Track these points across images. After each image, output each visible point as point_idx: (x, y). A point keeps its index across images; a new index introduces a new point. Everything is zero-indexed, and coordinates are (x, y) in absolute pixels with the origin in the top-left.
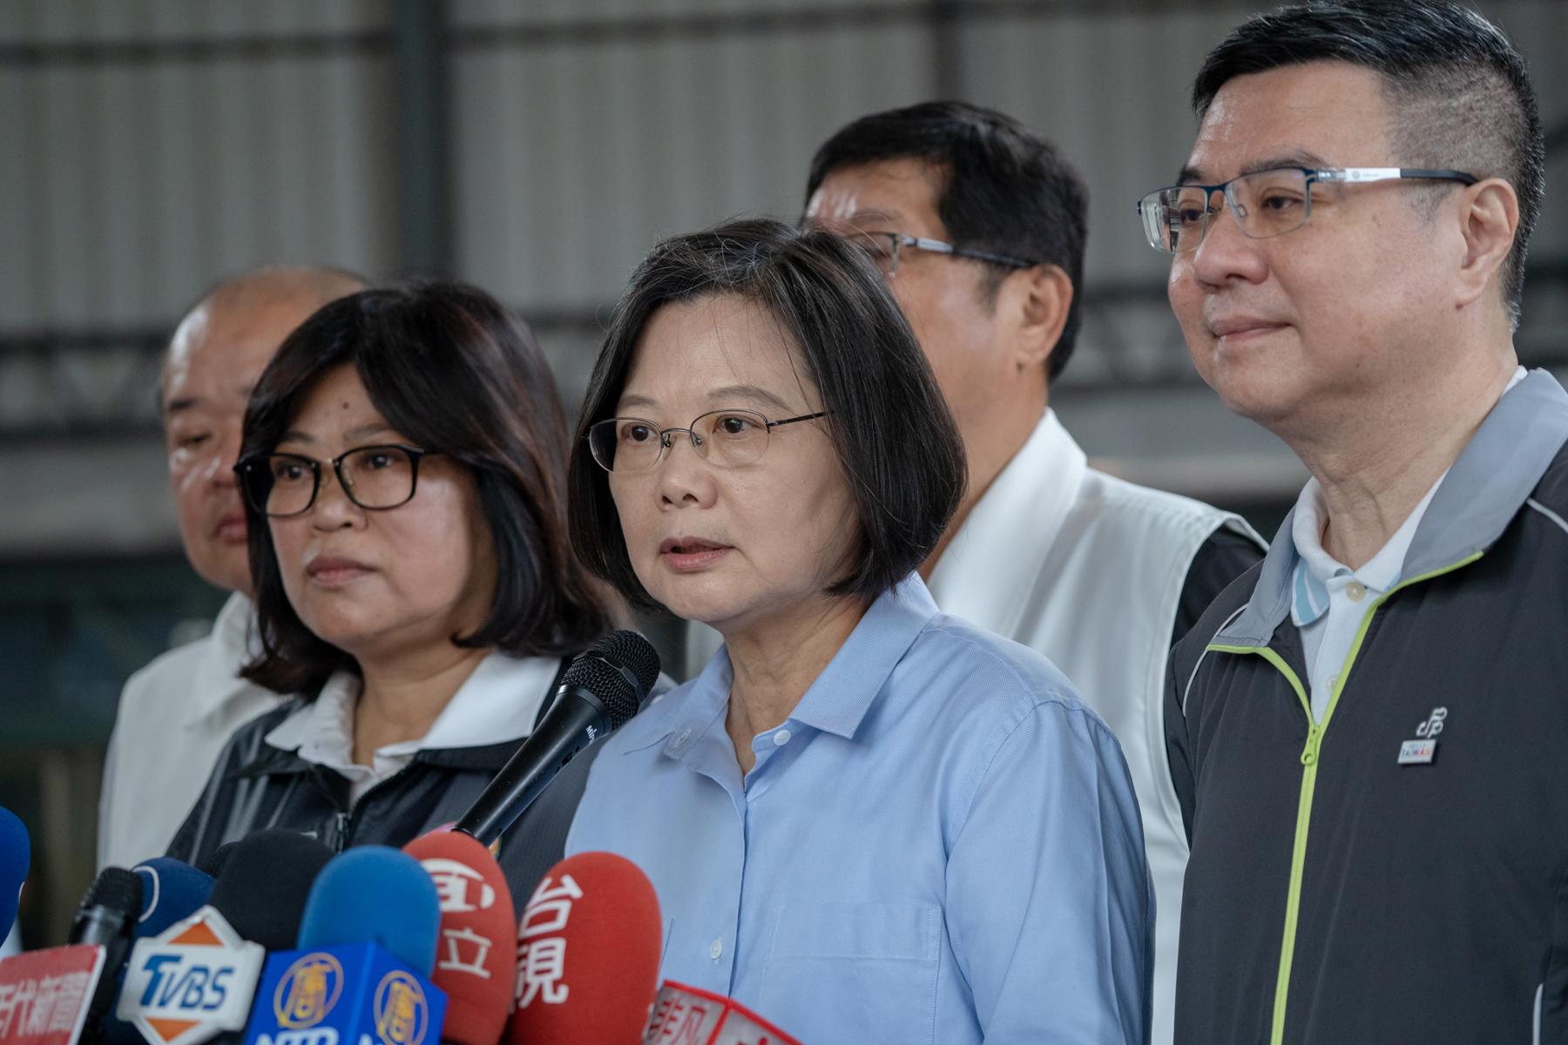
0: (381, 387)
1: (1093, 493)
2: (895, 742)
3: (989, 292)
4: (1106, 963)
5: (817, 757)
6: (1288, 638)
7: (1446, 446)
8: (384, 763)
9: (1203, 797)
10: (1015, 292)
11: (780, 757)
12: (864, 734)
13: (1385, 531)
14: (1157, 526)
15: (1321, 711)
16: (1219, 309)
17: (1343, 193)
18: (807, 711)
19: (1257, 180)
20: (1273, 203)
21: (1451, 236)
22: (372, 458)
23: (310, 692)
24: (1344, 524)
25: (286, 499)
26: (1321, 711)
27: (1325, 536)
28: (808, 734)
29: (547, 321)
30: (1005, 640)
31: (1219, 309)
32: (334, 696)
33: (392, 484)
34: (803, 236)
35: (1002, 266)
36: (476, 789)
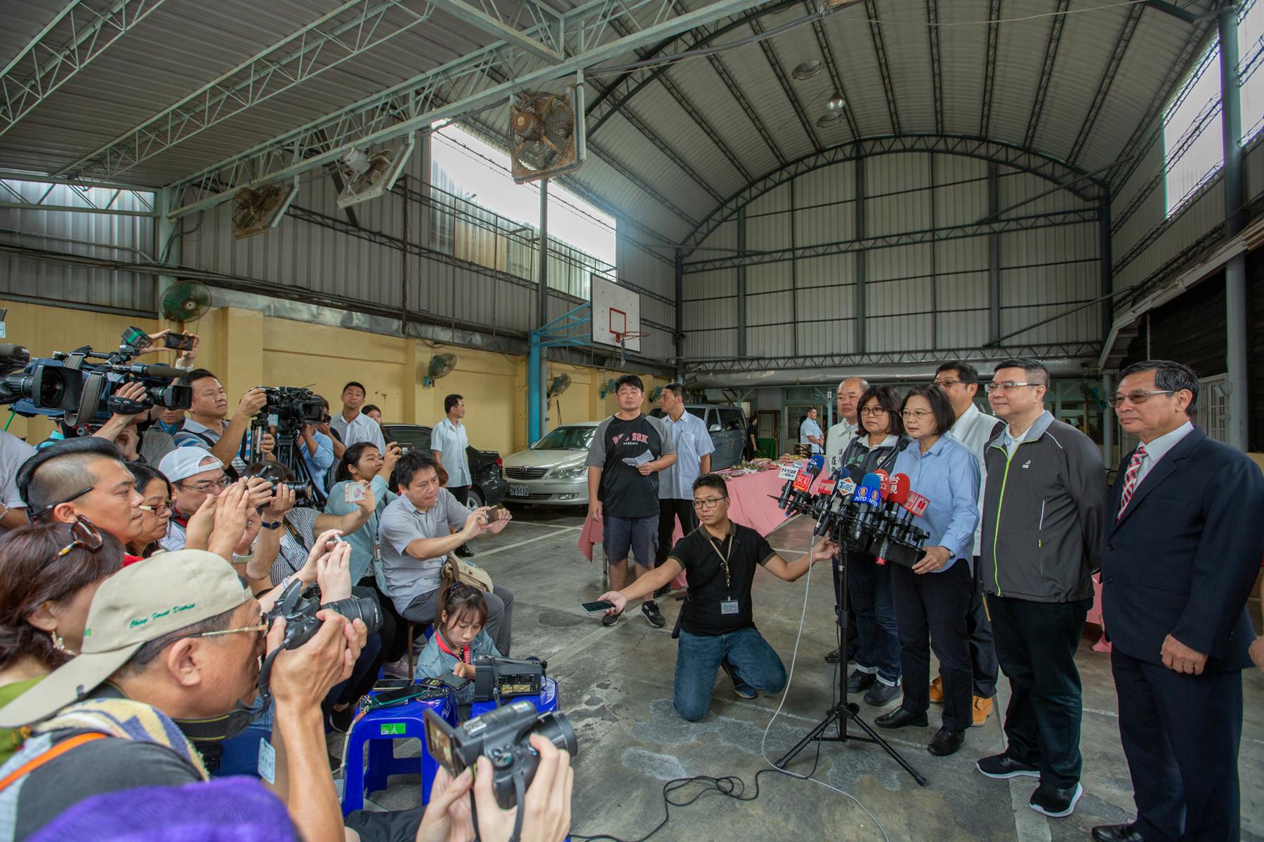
0: (879, 399)
1: (979, 417)
2: (943, 455)
3: (966, 387)
4: (973, 488)
5: (931, 456)
6: (1004, 447)
7: (1032, 422)
8: (875, 447)
9: (990, 466)
10: (970, 386)
11: (926, 456)
12: (939, 454)
13: (1021, 434)
14: (989, 421)
15: (1010, 458)
16: (996, 401)
17: (1017, 386)
18: (930, 450)
19: (924, 770)
20: (1006, 387)
21: (1034, 393)
22: (877, 409)
23: (864, 436)
24: (1014, 431)
25: (864, 413)
26: (1010, 458)
27: (1011, 432)
28: (930, 453)
29: (806, 665)
30: (960, 442)
31: (996, 401)
32: (867, 436)
33: (879, 413)
34: (929, 409)
35: (968, 384)
36: (888, 453)
